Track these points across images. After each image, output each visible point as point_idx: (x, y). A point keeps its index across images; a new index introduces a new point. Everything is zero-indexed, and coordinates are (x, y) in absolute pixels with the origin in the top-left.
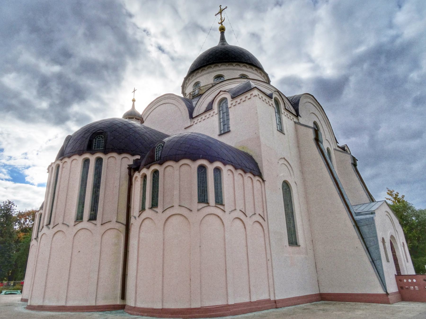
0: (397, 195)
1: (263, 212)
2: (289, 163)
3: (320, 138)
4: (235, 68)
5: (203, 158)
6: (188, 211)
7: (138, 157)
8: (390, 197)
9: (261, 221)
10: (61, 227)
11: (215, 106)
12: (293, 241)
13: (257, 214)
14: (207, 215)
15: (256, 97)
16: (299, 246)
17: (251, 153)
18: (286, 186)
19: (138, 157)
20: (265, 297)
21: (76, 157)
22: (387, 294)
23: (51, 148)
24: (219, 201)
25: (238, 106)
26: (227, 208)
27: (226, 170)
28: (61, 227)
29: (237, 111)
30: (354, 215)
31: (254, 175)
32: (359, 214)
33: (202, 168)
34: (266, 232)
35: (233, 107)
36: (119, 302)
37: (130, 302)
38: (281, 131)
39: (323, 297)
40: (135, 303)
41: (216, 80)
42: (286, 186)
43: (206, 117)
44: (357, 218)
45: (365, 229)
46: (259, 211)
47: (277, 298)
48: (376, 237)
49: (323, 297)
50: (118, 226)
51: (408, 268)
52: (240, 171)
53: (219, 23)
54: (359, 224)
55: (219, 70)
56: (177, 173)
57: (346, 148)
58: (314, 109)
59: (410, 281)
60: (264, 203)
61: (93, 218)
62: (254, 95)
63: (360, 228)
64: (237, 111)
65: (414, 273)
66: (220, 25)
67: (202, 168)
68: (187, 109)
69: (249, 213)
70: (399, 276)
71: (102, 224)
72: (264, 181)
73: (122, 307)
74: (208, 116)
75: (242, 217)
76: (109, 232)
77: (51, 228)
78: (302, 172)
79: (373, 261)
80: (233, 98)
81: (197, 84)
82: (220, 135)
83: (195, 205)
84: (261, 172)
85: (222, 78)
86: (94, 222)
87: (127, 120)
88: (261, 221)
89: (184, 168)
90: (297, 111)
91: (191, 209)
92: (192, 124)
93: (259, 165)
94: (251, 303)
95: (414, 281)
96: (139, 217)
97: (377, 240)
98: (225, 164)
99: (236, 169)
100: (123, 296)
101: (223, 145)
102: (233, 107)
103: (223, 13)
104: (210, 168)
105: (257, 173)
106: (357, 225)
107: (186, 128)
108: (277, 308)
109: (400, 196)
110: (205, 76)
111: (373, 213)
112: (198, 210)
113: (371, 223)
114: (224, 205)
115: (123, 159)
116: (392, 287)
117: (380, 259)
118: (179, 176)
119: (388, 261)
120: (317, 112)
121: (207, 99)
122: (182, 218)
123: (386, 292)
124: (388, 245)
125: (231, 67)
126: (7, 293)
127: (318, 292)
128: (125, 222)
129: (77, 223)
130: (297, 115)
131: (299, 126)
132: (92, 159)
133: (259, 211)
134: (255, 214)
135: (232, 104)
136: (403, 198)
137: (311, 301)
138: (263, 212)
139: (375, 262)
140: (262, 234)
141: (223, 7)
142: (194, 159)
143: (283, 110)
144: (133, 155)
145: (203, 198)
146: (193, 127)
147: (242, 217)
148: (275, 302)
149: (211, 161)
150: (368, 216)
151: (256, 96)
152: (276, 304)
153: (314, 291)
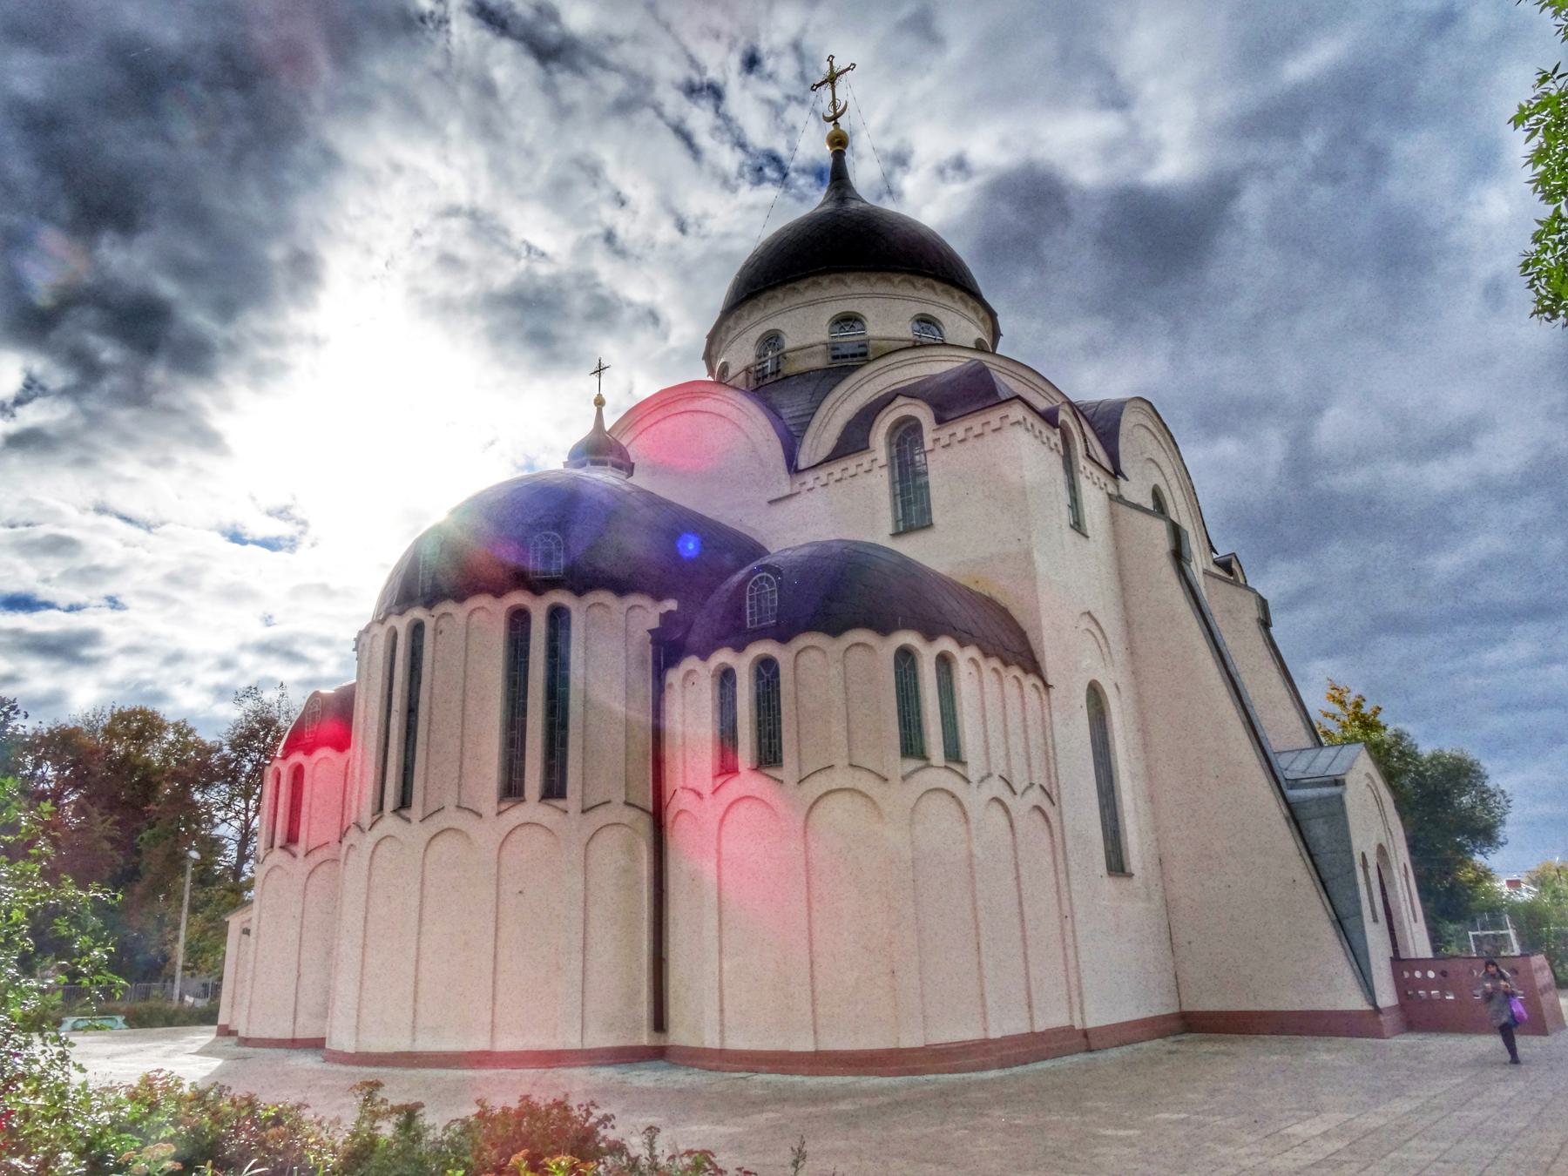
0: (1358, 705)
1: (1049, 777)
2: (1101, 629)
3: (1185, 551)
4: (899, 291)
5: (907, 626)
6: (878, 782)
7: (671, 605)
8: (1336, 709)
9: (1046, 805)
10: (452, 818)
11: (879, 437)
12: (1117, 865)
13: (1036, 787)
14: (928, 791)
15: (1017, 427)
16: (1131, 875)
17: (1003, 600)
18: (1095, 693)
19: (671, 605)
20: (1058, 1019)
21: (484, 601)
22: (1377, 1010)
23: (385, 566)
24: (954, 753)
25: (957, 448)
26: (974, 769)
27: (964, 658)
28: (452, 818)
29: (950, 458)
30: (1283, 784)
31: (1026, 672)
32: (1295, 783)
33: (905, 657)
34: (1058, 839)
35: (938, 449)
36: (645, 1038)
37: (680, 1035)
38: (1078, 526)
39: (1191, 1024)
40: (722, 1039)
41: (837, 328)
42: (1095, 693)
43: (846, 474)
44: (1294, 794)
45: (1318, 830)
46: (1039, 777)
47: (1090, 1024)
48: (1349, 851)
49: (1191, 1024)
50: (630, 815)
51: (1419, 943)
52: (995, 663)
53: (828, 120)
54: (1301, 814)
55: (845, 297)
56: (835, 671)
57: (1234, 566)
58: (1154, 449)
59: (1418, 974)
60: (1050, 756)
61: (554, 790)
62: (1012, 419)
63: (1303, 825)
64: (950, 458)
65: (1430, 955)
66: (830, 127)
67: (905, 657)
68: (773, 436)
69: (1019, 783)
70: (1398, 962)
71: (583, 812)
72: (1047, 686)
73: (658, 1054)
74: (852, 470)
75: (1006, 796)
76: (605, 833)
77: (415, 820)
78: (1132, 651)
79: (1340, 922)
80: (940, 421)
81: (772, 340)
82: (896, 534)
83: (897, 765)
84: (1038, 658)
85: (857, 326)
86: (560, 803)
87: (580, 472)
88: (1046, 805)
89: (857, 654)
90: (1114, 457)
91: (885, 773)
92: (796, 488)
93: (1031, 636)
94: (1034, 1036)
95: (1431, 974)
96: (714, 793)
97: (1352, 857)
98: (962, 644)
99: (986, 655)
100: (659, 1022)
101: (909, 569)
102: (938, 449)
103: (841, 84)
104: (927, 656)
105: (1028, 665)
106: (1295, 816)
107: (771, 502)
108: (1090, 1050)
109: (1367, 709)
110: (799, 314)
111: (1338, 782)
112: (904, 778)
113: (1335, 811)
114: (964, 763)
115: (632, 613)
116: (1387, 996)
117: (1359, 914)
118: (834, 675)
119: (1376, 920)
120: (1162, 458)
121: (841, 410)
122: (859, 800)
123: (1374, 1004)
124: (1373, 873)
125: (881, 288)
126: (81, 1024)
127: (1174, 1009)
128: (650, 807)
129: (503, 807)
130: (1116, 473)
131: (1122, 509)
132: (743, 664)
133: (1039, 777)
134: (1032, 785)
135: (936, 440)
136: (1375, 714)
137: (1163, 1035)
138: (1049, 777)
139: (1345, 925)
140: (1046, 840)
141: (839, 64)
142: (884, 628)
143: (1082, 462)
144: (658, 597)
145: (912, 746)
146: (797, 498)
147: (1006, 796)
148: (1085, 1033)
149: (930, 636)
150: (1326, 791)
151: (1018, 423)
152: (1087, 1040)
153: (1159, 1005)
